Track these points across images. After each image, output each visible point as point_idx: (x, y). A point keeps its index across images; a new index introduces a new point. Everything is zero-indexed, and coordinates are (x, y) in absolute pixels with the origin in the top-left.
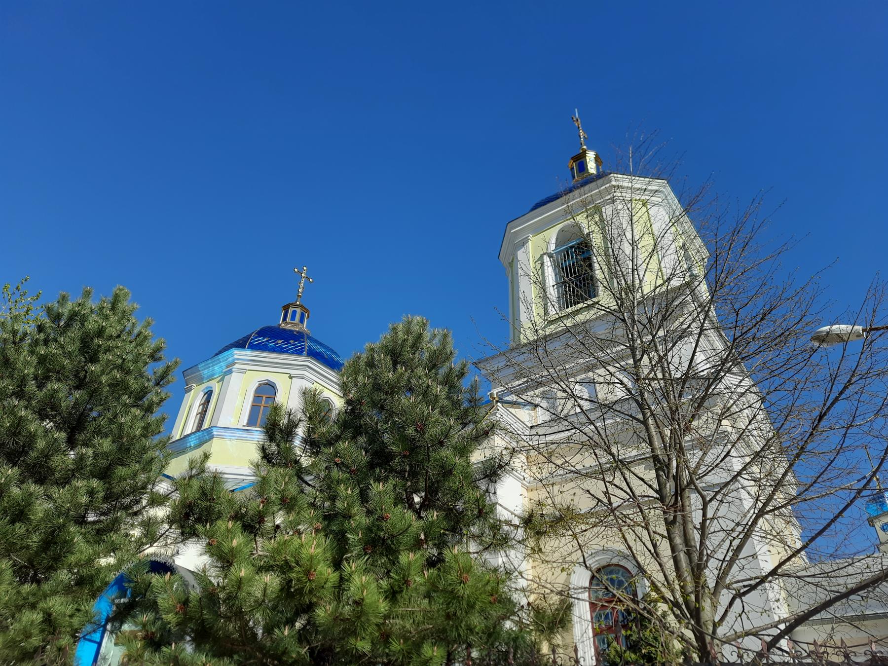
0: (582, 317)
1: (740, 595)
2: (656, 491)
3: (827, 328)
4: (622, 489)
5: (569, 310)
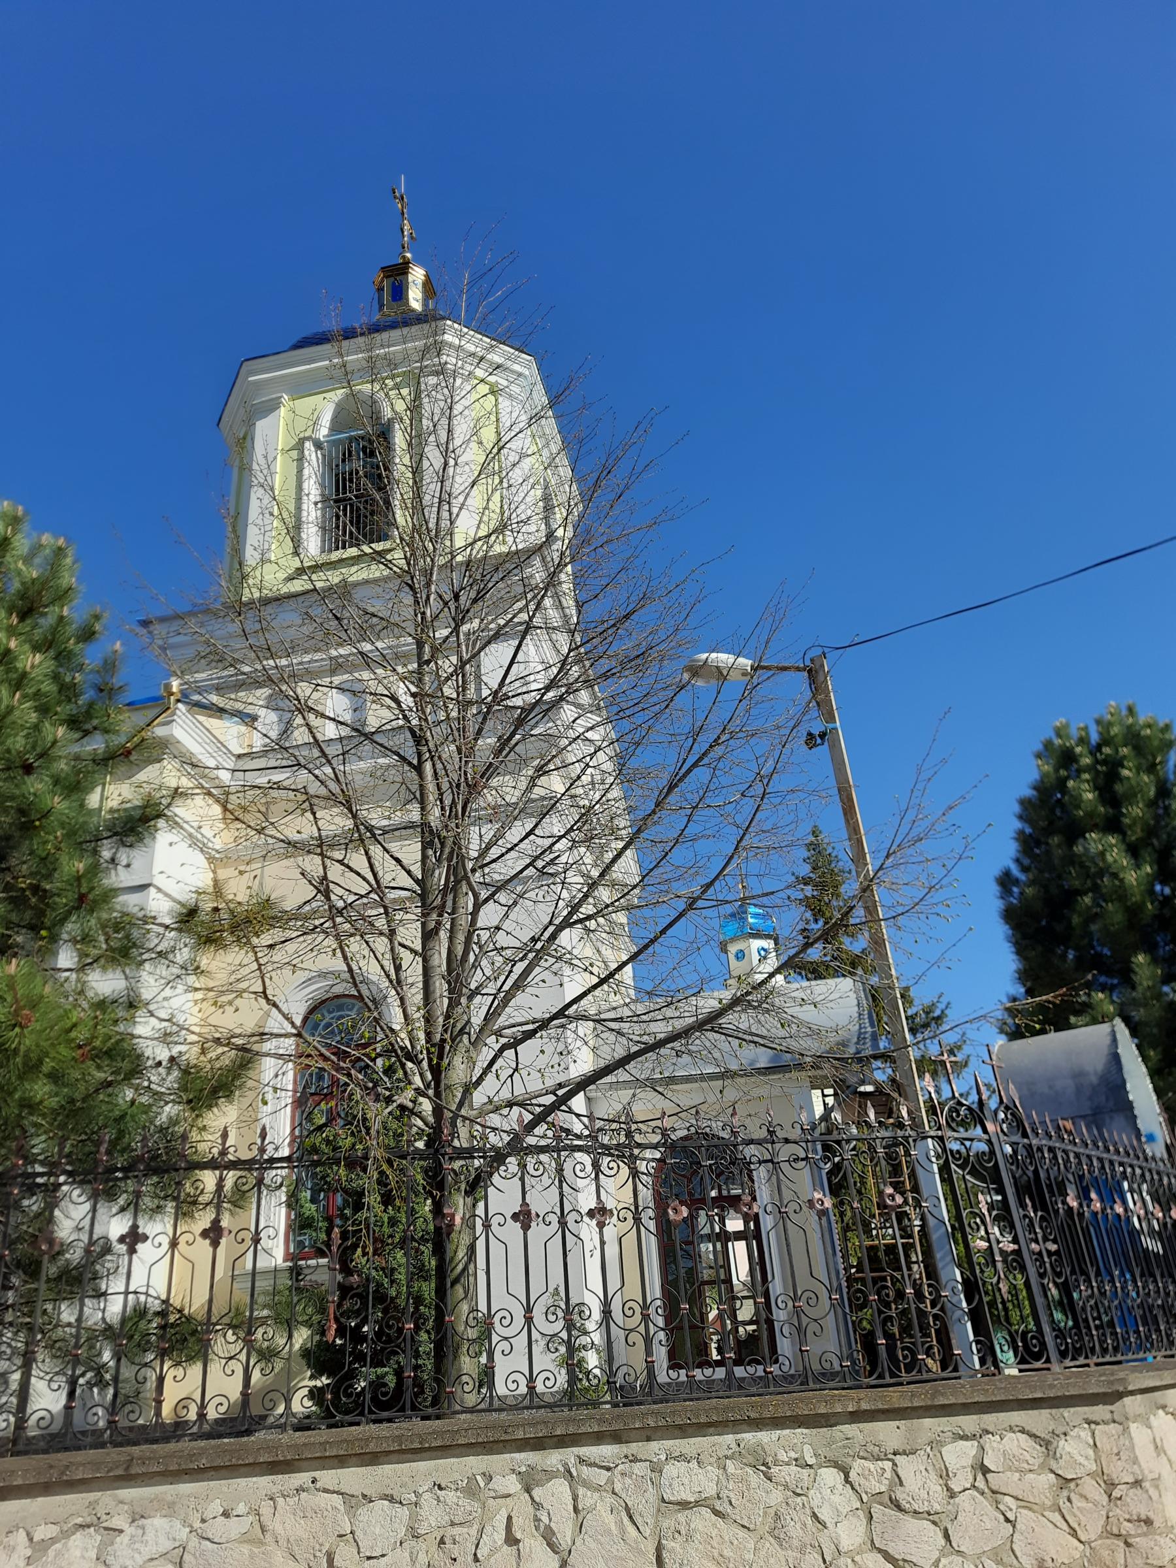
0: (356, 574)
1: (515, 1044)
2: (417, 881)
3: (704, 656)
4: (358, 874)
5: (335, 556)
